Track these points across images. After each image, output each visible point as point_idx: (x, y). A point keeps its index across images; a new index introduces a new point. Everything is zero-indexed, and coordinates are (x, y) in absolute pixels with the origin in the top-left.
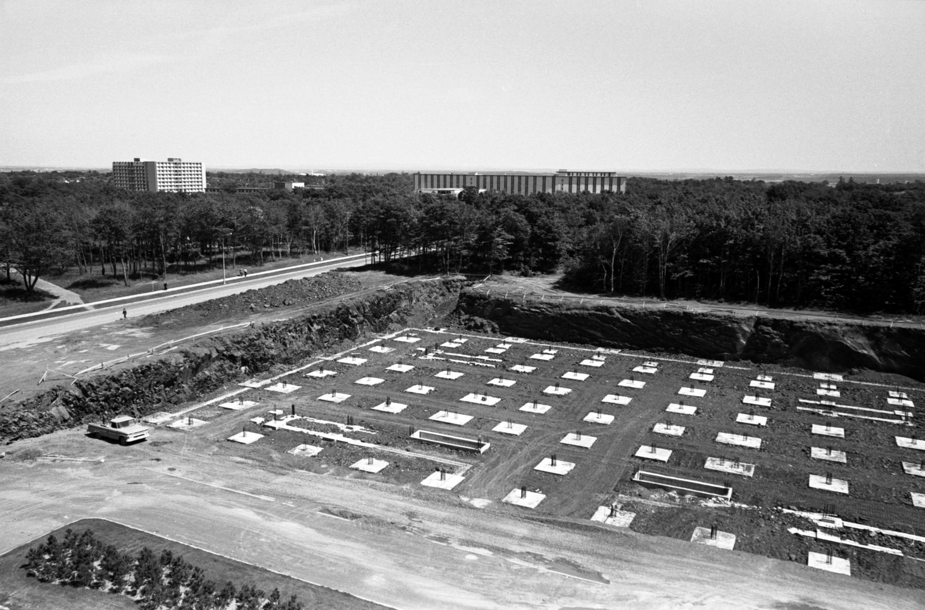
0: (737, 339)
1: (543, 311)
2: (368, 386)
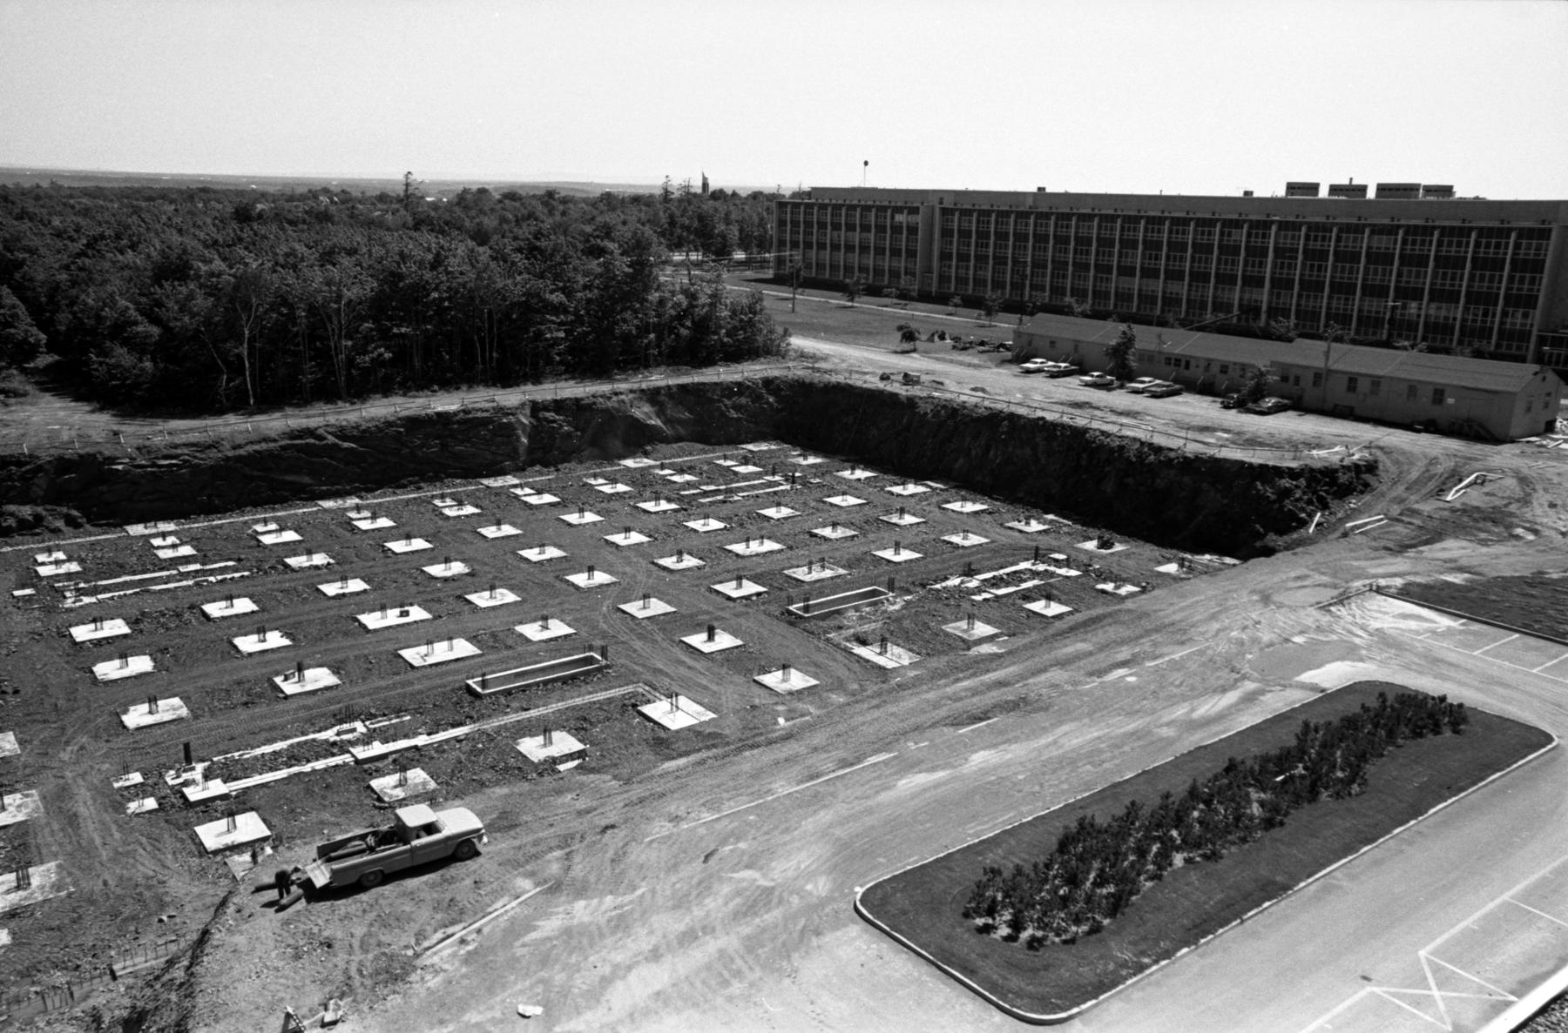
0: (518, 439)
1: (187, 461)
2: (961, 513)
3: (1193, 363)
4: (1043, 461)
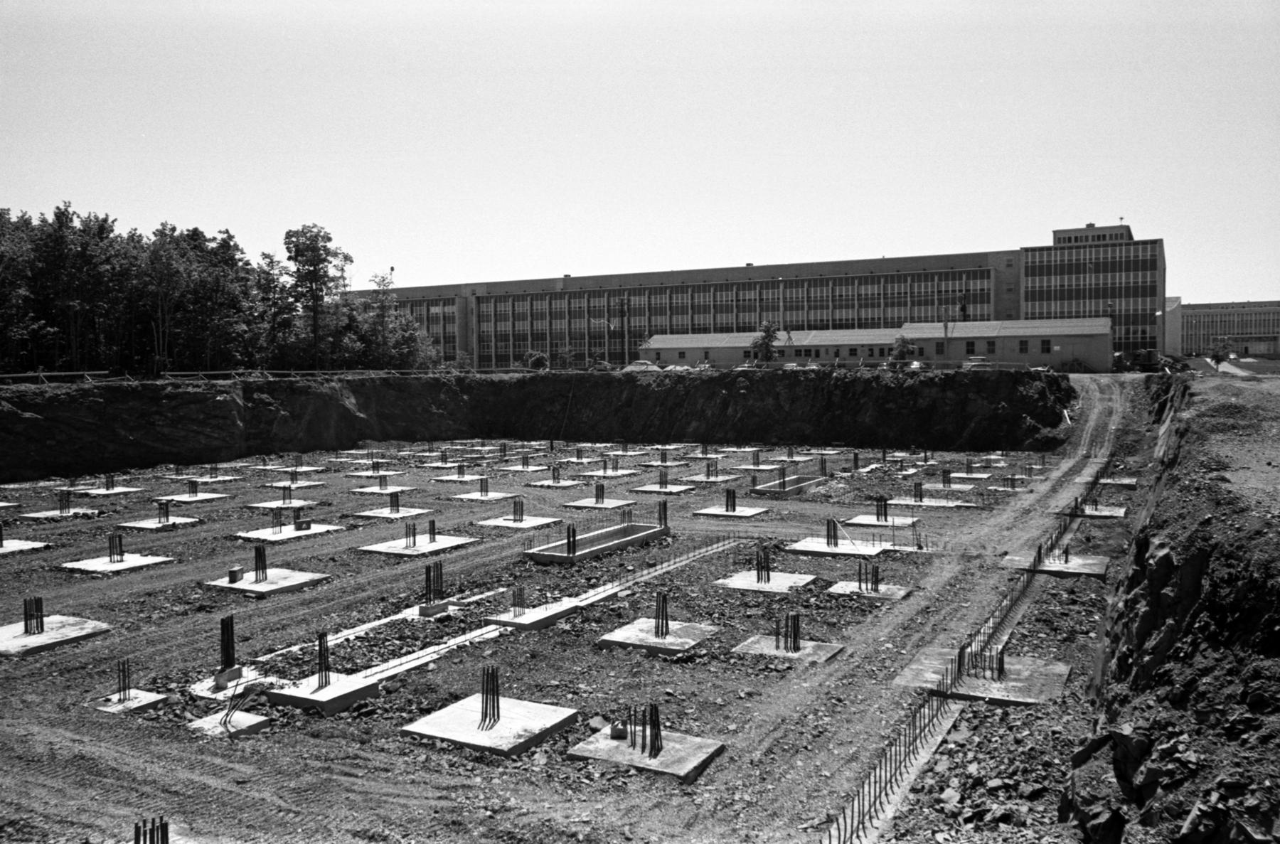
3: (822, 352)
4: (787, 408)
